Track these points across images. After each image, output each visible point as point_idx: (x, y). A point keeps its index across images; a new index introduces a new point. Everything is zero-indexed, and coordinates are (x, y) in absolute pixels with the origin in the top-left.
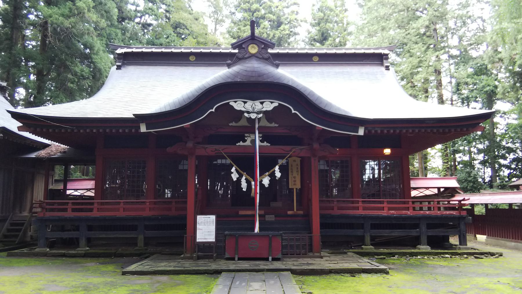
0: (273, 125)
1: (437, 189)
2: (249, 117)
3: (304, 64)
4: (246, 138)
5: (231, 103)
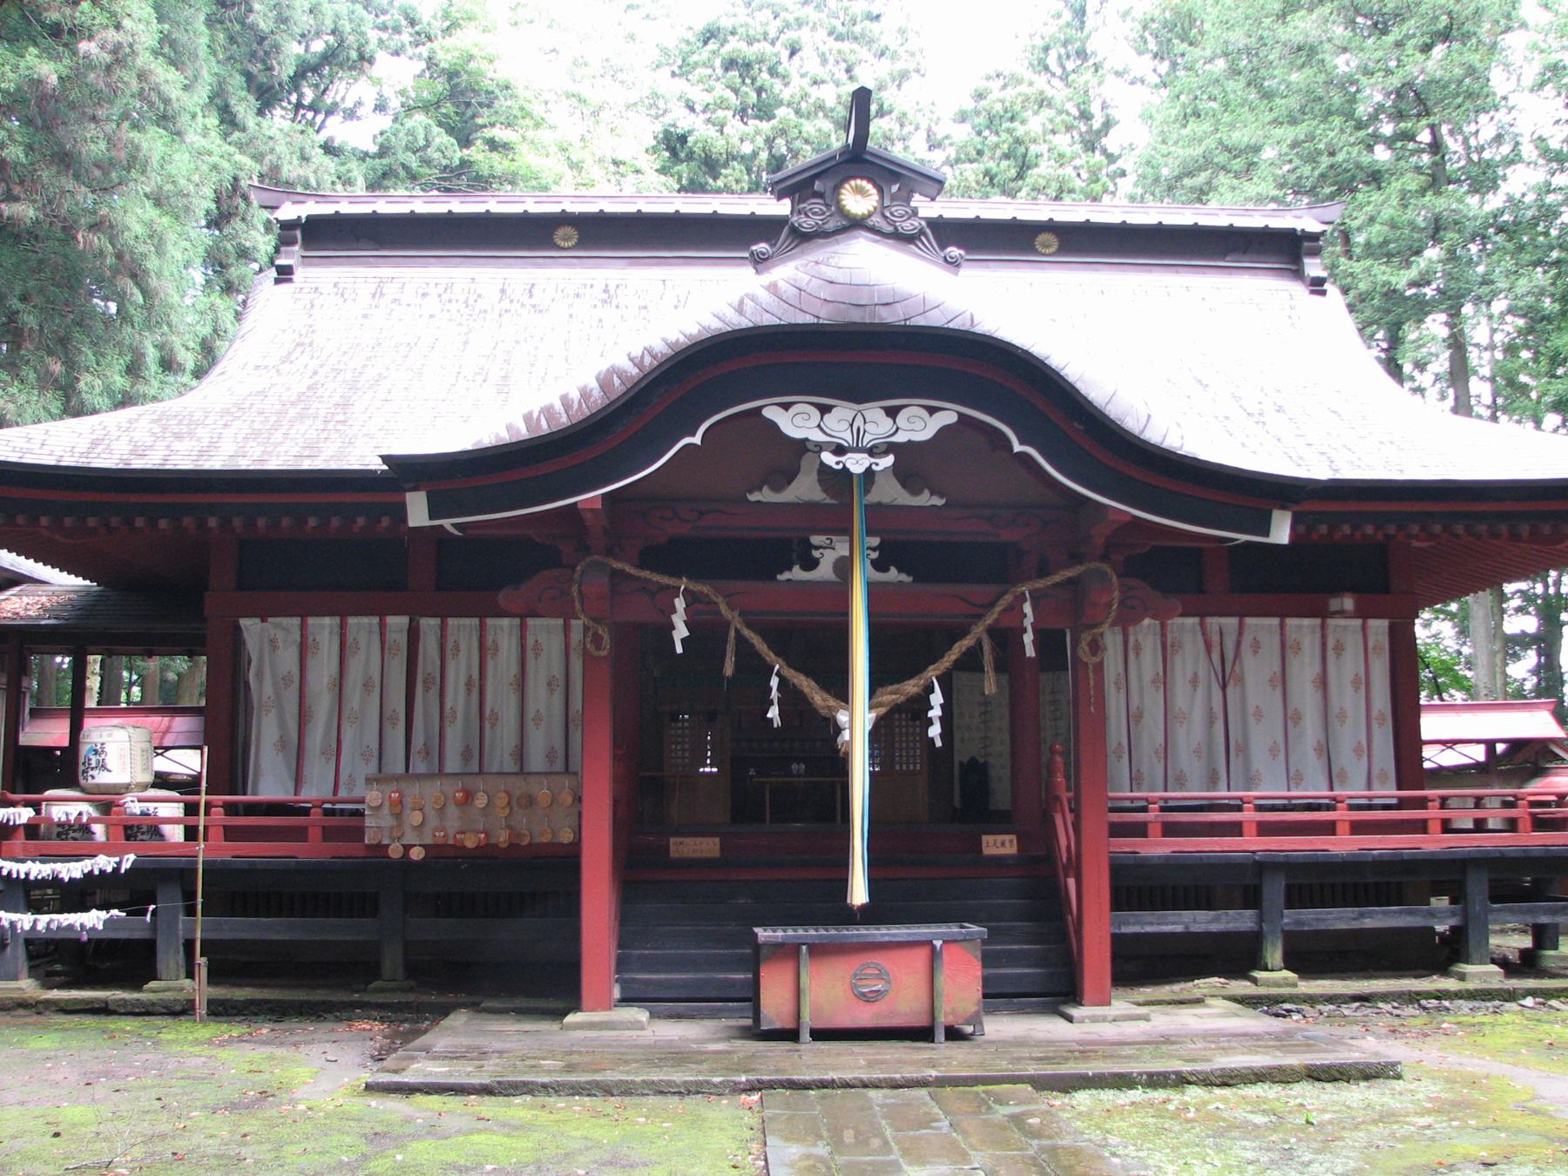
0: (926, 499)
1: (1482, 747)
2: (840, 466)
3: (1027, 264)
4: (816, 554)
5: (767, 413)
